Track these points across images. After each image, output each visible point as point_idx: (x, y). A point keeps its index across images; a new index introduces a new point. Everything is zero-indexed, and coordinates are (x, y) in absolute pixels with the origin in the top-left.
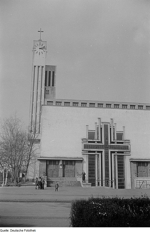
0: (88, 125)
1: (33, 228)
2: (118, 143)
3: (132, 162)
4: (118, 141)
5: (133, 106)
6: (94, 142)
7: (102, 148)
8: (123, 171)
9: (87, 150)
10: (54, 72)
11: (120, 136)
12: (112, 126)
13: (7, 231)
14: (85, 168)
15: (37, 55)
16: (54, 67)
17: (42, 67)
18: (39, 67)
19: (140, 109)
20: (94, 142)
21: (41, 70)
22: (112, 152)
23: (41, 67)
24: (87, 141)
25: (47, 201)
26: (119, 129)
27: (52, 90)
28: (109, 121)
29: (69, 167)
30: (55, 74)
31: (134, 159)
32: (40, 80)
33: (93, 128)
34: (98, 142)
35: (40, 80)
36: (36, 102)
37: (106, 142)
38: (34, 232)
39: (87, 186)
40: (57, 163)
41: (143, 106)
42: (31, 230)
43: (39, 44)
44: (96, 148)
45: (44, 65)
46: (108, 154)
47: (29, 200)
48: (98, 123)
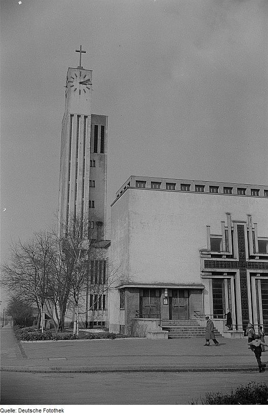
1: (59, 407)
4: (262, 255)
6: (220, 256)
7: (236, 267)
9: (210, 270)
10: (103, 128)
13: (13, 411)
14: (207, 302)
15: (74, 96)
16: (103, 118)
17: (86, 117)
18: (79, 116)
19: (199, 191)
20: (220, 256)
21: (83, 123)
22: (234, 274)
24: (208, 254)
27: (100, 160)
28: (245, 219)
29: (178, 301)
30: (106, 131)
32: (81, 140)
34: (228, 256)
35: (81, 140)
37: (242, 256)
38: (61, 413)
39: (238, 336)
40: (157, 295)
41: (217, 187)
42: (55, 410)
43: (78, 75)
44: (225, 267)
45: (88, 114)
46: (246, 277)
47: (244, 366)
48: (226, 221)
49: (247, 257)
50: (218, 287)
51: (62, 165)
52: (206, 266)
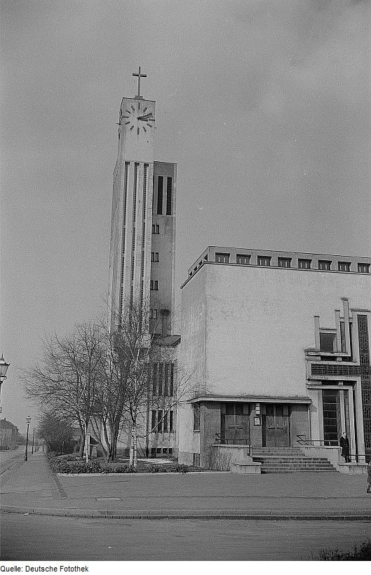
0: (318, 315)
1: (81, 564)
5: (305, 263)
6: (334, 358)
7: (356, 374)
9: (319, 377)
10: (170, 180)
13: (18, 569)
15: (130, 136)
16: (170, 167)
17: (137, 164)
18: (137, 164)
19: (304, 267)
20: (334, 358)
22: (352, 383)
23: (133, 164)
29: (275, 421)
30: (174, 185)
31: (285, 399)
33: (330, 323)
34: (344, 359)
36: (133, 253)
38: (85, 573)
40: (245, 412)
42: (76, 568)
43: (136, 107)
44: (341, 374)
45: (150, 161)
48: (342, 310)
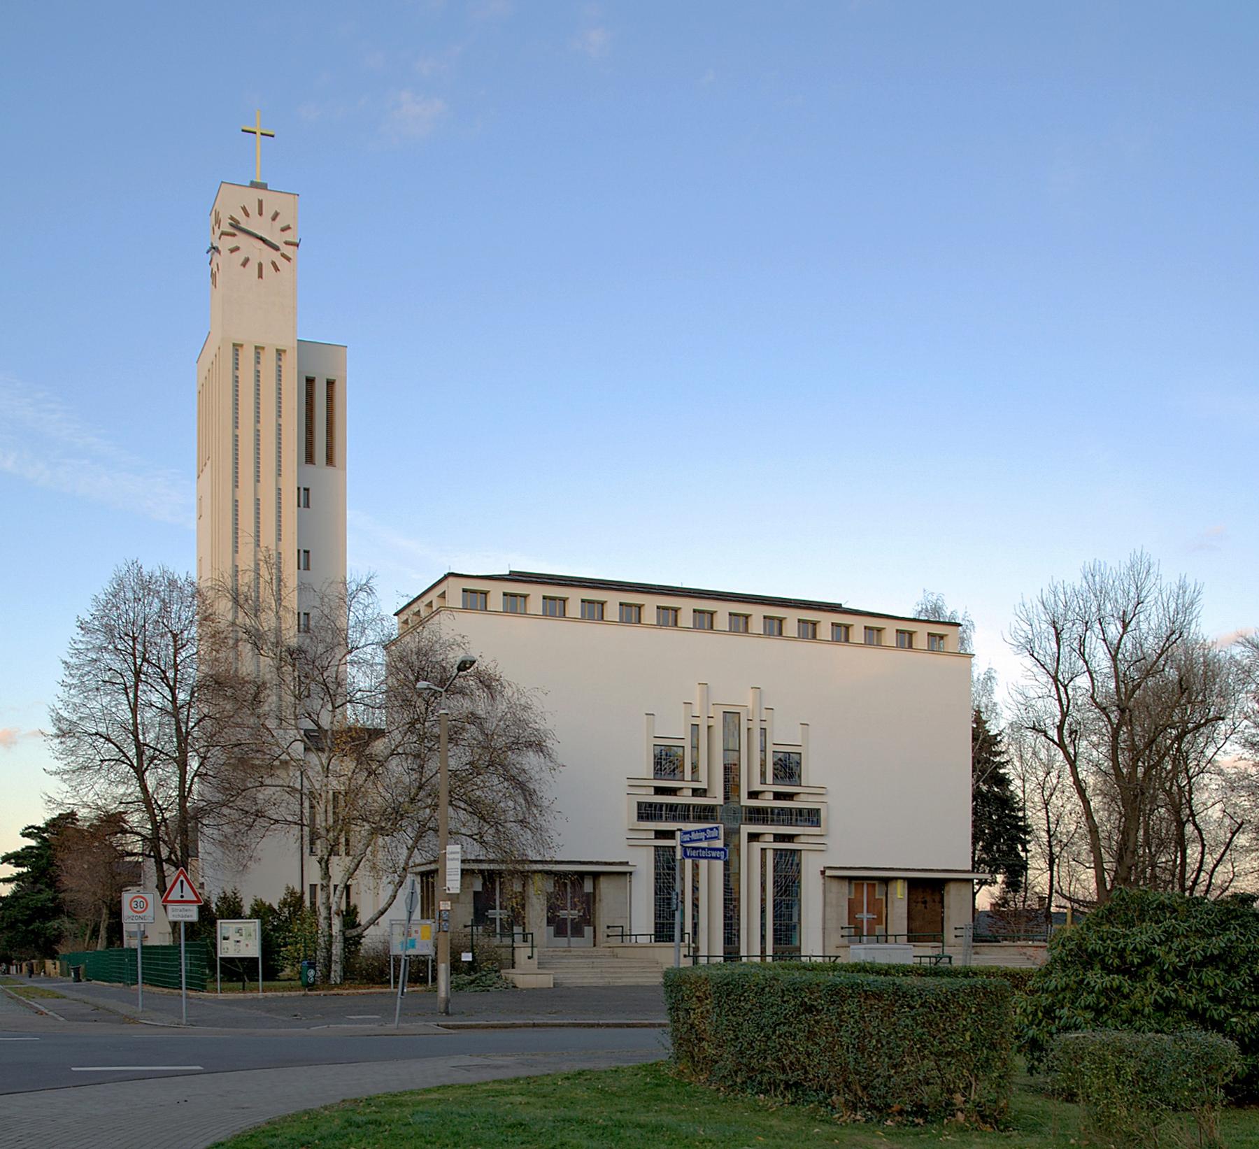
2: (777, 796)
3: (830, 876)
6: (673, 791)
7: (726, 798)
8: (658, 877)
11: (787, 768)
12: (757, 720)
18: (258, 349)
20: (779, 838)
25: (520, 1026)
26: (784, 735)
28: (748, 699)
34: (696, 792)
49: (744, 794)
50: (666, 869)
51: (497, 1086)
52: (641, 817)
